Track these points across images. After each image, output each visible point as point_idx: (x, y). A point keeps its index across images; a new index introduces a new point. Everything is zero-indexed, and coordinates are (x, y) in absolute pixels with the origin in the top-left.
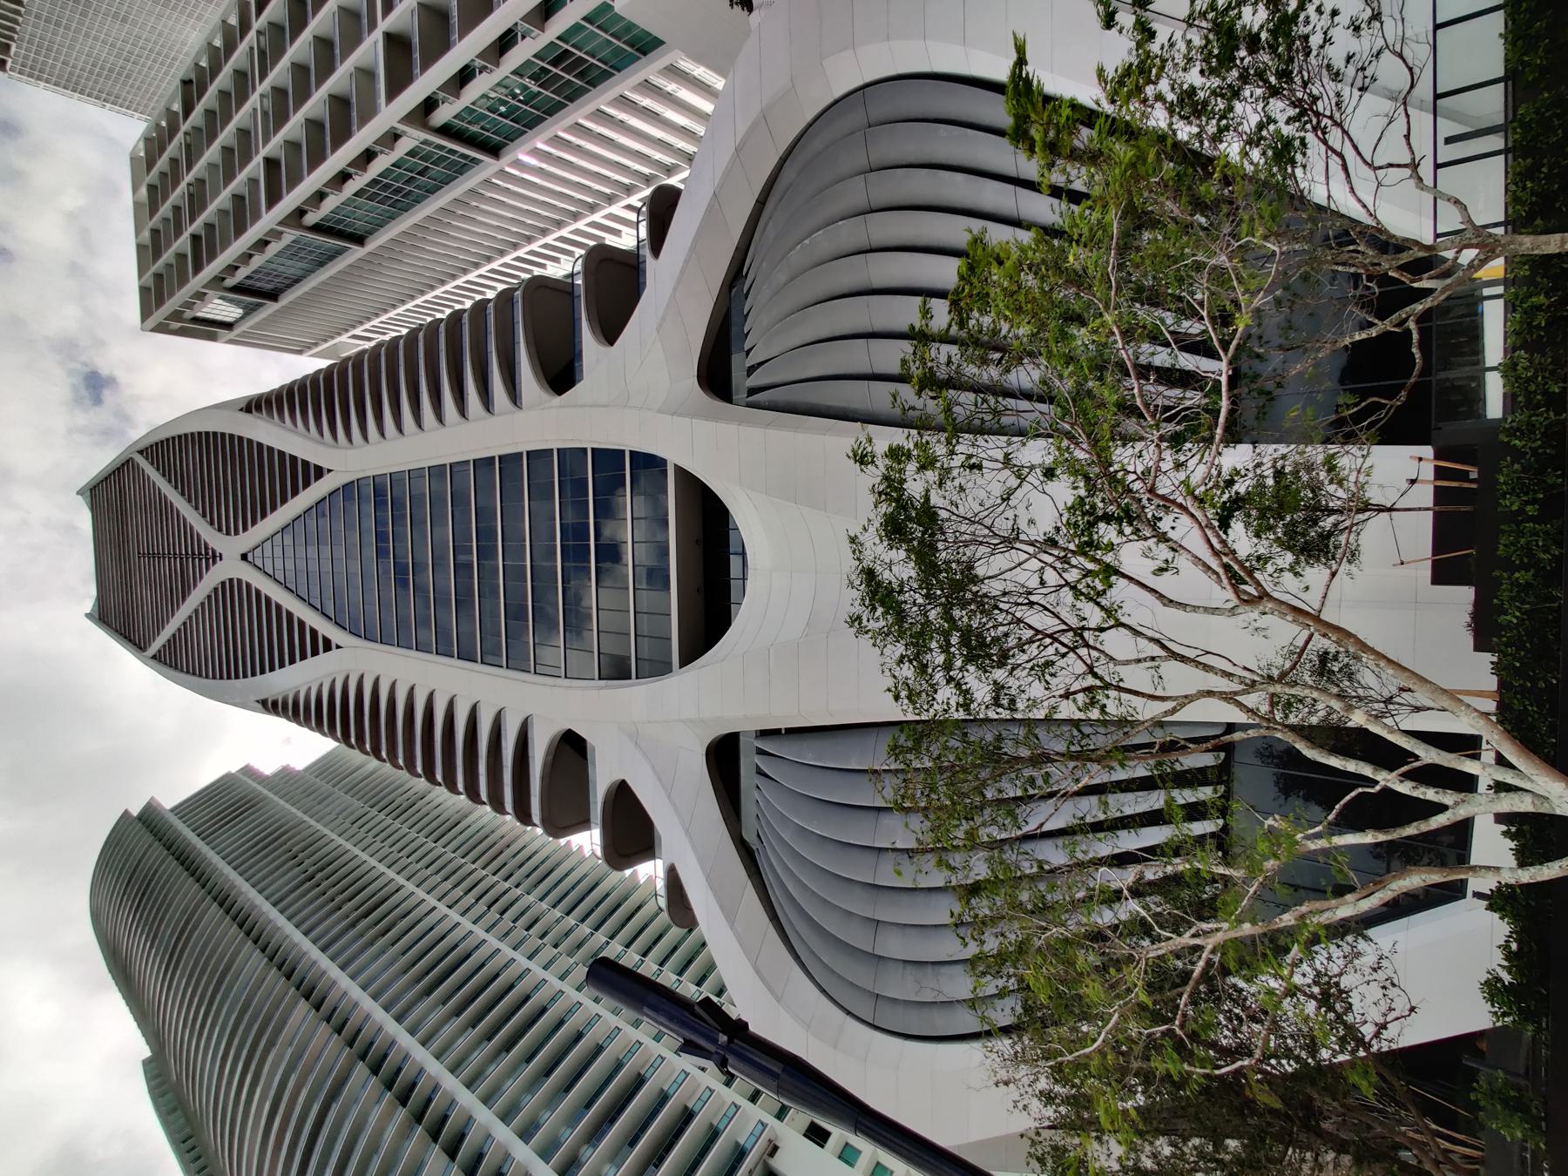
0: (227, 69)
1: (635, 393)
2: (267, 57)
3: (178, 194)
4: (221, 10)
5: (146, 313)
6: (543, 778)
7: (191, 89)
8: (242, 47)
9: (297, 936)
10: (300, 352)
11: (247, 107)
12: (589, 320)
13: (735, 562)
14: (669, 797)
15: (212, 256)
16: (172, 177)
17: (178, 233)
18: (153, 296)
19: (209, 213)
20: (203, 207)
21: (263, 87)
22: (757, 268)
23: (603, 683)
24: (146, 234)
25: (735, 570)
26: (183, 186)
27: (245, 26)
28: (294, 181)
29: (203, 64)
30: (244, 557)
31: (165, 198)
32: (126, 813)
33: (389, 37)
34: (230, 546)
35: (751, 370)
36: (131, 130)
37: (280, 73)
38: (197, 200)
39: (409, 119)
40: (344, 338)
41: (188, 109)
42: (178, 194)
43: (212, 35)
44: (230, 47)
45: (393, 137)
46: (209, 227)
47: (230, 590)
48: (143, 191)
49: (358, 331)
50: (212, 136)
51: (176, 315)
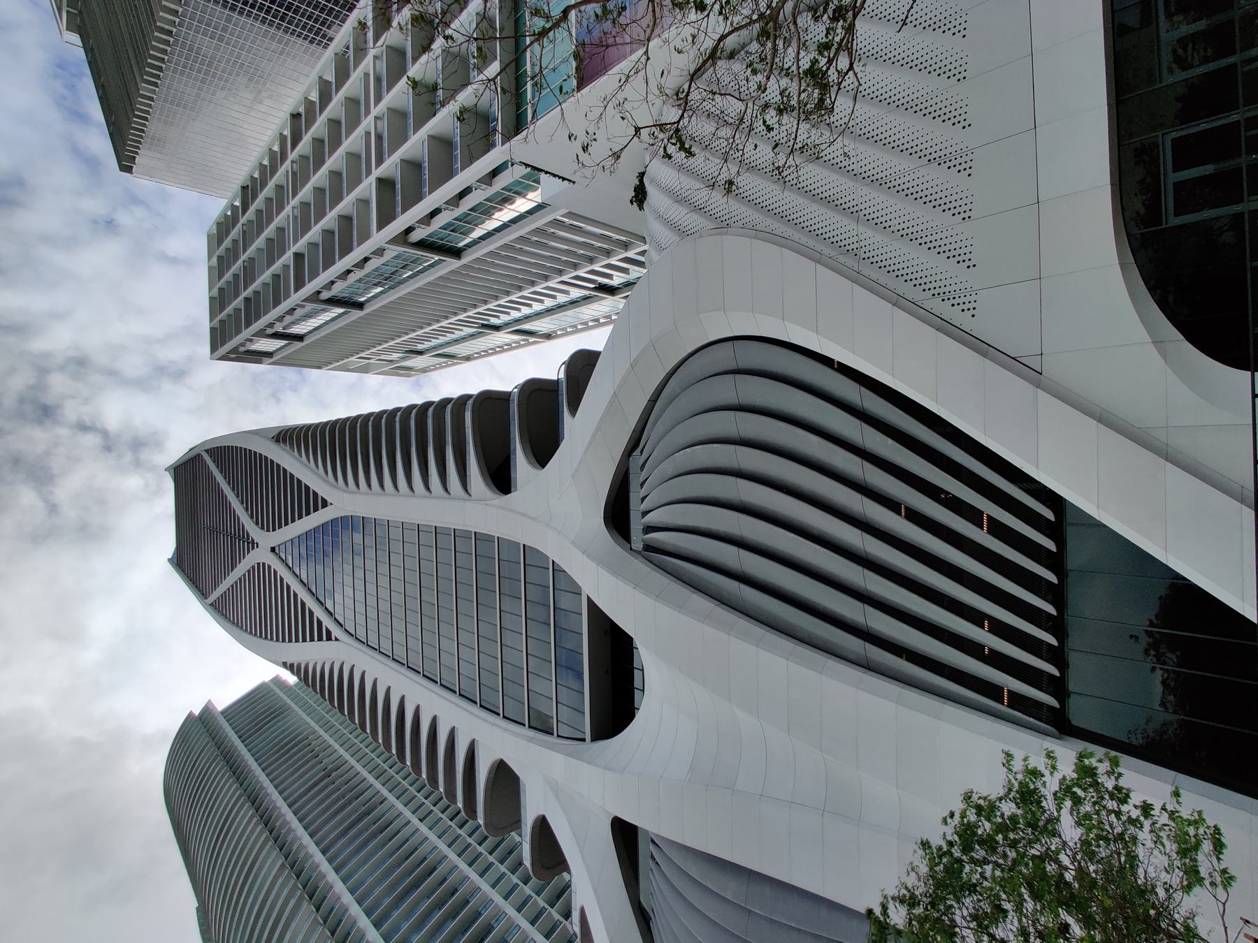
0: (271, 184)
1: (554, 510)
2: (299, 178)
3: (237, 267)
4: (304, 88)
5: (214, 348)
6: (486, 791)
7: (248, 192)
8: (281, 171)
9: (306, 840)
10: (320, 368)
11: (283, 214)
12: (522, 442)
13: (637, 674)
14: (582, 852)
15: (258, 318)
16: (233, 254)
17: (237, 295)
18: (219, 337)
19: (256, 285)
20: (253, 280)
21: (295, 202)
22: (651, 435)
23: (532, 733)
24: (215, 291)
25: (637, 684)
26: (240, 262)
27: (284, 156)
28: (314, 274)
29: (256, 176)
30: (273, 550)
31: (229, 268)
32: (191, 715)
33: (380, 181)
34: (265, 539)
35: (645, 513)
36: (216, 206)
37: (306, 193)
38: (250, 273)
39: (394, 241)
40: (352, 359)
41: (245, 207)
42: (237, 267)
43: (253, 171)
44: (274, 169)
45: (380, 252)
46: (256, 293)
47: (261, 567)
48: (215, 259)
49: (362, 355)
50: (260, 230)
51: (235, 350)
